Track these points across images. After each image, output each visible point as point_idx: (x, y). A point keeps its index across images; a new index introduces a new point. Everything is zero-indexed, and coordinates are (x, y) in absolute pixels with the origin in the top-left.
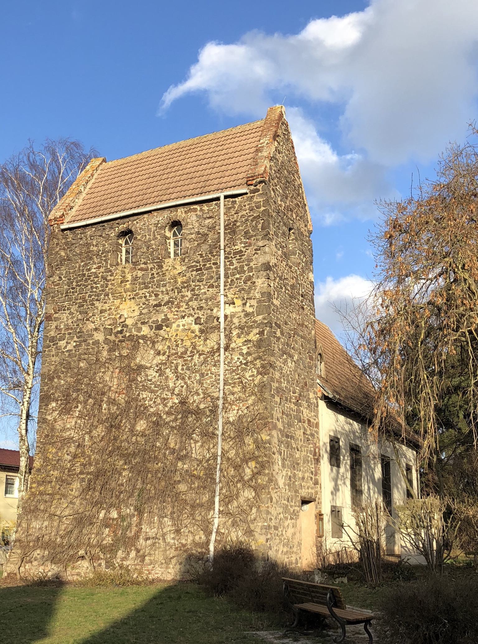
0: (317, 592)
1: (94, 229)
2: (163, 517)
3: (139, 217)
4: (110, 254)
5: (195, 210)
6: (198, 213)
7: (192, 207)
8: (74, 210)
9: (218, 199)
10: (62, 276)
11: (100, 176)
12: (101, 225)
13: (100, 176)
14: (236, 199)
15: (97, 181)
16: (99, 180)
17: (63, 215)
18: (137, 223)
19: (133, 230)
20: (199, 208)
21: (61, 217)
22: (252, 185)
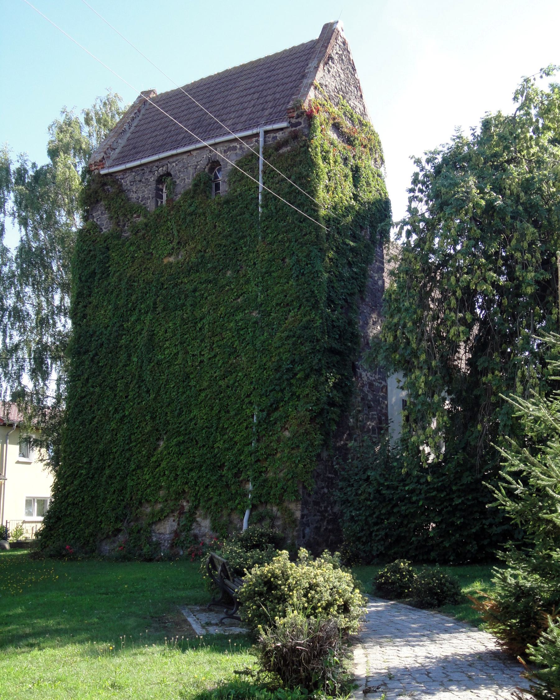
0: (414, 636)
1: (134, 174)
2: (224, 537)
3: (178, 158)
4: (149, 201)
5: (235, 148)
6: (238, 151)
7: (231, 146)
8: (117, 151)
9: (257, 135)
10: (103, 227)
11: (148, 112)
12: (141, 168)
13: (148, 112)
14: (277, 135)
15: (144, 117)
16: (146, 116)
17: (103, 158)
18: (177, 165)
19: (172, 173)
20: (238, 146)
21: (101, 161)
22: (293, 117)
